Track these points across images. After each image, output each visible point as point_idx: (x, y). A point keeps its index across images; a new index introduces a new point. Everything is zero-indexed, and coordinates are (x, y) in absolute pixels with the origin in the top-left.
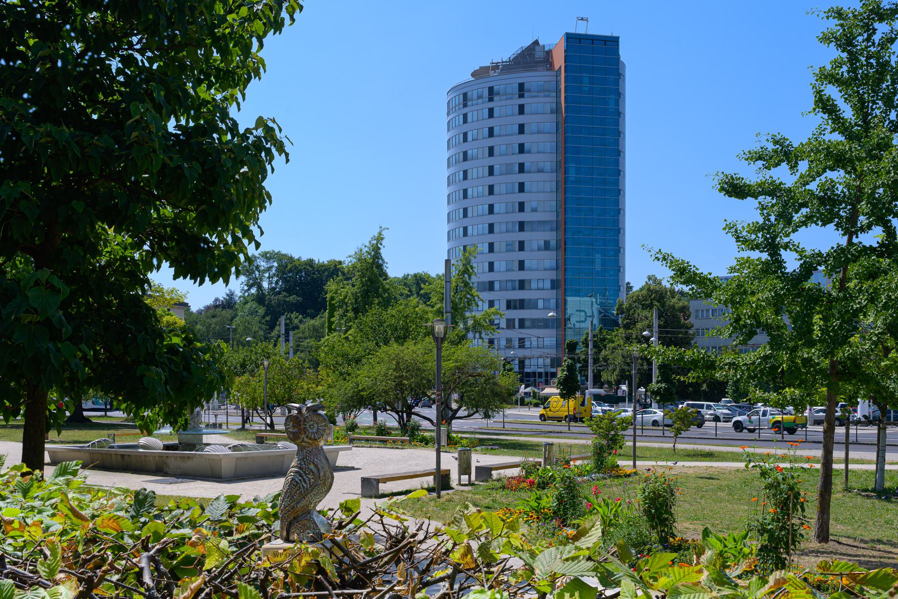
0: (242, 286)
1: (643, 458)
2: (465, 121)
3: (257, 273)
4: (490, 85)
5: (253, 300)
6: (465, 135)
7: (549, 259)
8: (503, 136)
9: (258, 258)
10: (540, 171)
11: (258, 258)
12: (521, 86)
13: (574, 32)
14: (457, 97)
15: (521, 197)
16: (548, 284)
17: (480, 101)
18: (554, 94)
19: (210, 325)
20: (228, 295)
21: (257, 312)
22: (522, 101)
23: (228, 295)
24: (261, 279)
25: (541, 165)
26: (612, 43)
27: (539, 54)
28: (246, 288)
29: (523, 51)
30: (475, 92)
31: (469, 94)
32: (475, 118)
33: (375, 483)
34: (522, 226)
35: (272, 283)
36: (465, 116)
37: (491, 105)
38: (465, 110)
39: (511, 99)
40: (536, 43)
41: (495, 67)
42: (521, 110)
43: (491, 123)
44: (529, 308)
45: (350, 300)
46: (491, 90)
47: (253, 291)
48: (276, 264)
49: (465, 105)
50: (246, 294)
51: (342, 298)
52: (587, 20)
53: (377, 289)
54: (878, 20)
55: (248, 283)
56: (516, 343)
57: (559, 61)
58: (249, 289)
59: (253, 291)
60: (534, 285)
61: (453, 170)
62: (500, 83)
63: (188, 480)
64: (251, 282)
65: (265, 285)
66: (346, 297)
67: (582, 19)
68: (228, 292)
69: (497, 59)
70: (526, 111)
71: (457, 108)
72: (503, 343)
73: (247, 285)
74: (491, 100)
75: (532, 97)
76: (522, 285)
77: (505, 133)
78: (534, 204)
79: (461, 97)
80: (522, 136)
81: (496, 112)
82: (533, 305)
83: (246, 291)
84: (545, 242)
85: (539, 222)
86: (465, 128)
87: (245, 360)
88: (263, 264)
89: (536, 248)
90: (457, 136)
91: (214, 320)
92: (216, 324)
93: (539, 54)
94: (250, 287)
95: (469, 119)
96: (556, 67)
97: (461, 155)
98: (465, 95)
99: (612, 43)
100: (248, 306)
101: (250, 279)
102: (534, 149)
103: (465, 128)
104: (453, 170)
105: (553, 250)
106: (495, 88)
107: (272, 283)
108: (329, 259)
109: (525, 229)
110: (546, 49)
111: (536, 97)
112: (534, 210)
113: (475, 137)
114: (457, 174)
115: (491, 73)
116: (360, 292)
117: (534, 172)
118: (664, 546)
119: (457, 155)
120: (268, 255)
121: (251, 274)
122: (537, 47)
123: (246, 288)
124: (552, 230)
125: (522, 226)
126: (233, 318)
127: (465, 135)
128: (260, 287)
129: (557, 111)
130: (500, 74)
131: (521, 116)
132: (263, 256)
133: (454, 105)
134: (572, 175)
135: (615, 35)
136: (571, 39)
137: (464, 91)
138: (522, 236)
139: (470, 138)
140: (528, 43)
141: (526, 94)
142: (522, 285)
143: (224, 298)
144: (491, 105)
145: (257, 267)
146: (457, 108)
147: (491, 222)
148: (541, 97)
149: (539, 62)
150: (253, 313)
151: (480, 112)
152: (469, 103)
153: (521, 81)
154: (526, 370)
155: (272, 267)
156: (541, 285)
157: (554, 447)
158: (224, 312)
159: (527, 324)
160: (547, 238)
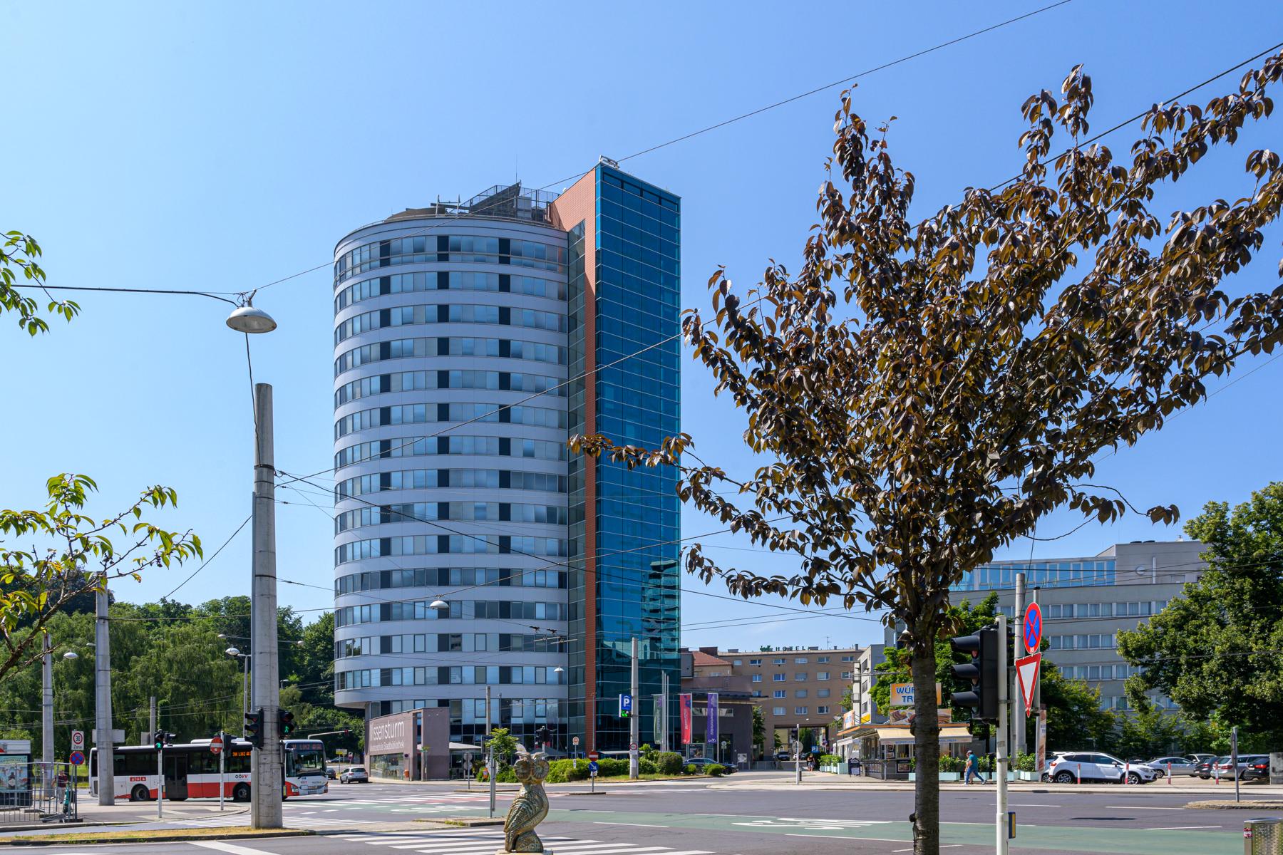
7: (550, 537)
12: (504, 245)
15: (505, 430)
16: (553, 580)
25: (542, 381)
34: (505, 479)
38: (385, 272)
42: (443, 281)
44: (519, 617)
46: (443, 242)
49: (385, 263)
54: (898, 610)
60: (528, 579)
70: (452, 284)
72: (469, 673)
75: (403, 263)
76: (505, 577)
78: (528, 445)
81: (395, 284)
82: (527, 611)
84: (549, 508)
89: (533, 517)
98: (385, 248)
102: (529, 351)
106: (451, 239)
111: (412, 262)
112: (529, 454)
125: (505, 479)
131: (443, 292)
134: (608, 397)
138: (506, 496)
141: (393, 260)
142: (505, 577)
148: (538, 268)
153: (505, 235)
154: (514, 721)
156: (540, 579)
159: (516, 643)
160: (553, 504)
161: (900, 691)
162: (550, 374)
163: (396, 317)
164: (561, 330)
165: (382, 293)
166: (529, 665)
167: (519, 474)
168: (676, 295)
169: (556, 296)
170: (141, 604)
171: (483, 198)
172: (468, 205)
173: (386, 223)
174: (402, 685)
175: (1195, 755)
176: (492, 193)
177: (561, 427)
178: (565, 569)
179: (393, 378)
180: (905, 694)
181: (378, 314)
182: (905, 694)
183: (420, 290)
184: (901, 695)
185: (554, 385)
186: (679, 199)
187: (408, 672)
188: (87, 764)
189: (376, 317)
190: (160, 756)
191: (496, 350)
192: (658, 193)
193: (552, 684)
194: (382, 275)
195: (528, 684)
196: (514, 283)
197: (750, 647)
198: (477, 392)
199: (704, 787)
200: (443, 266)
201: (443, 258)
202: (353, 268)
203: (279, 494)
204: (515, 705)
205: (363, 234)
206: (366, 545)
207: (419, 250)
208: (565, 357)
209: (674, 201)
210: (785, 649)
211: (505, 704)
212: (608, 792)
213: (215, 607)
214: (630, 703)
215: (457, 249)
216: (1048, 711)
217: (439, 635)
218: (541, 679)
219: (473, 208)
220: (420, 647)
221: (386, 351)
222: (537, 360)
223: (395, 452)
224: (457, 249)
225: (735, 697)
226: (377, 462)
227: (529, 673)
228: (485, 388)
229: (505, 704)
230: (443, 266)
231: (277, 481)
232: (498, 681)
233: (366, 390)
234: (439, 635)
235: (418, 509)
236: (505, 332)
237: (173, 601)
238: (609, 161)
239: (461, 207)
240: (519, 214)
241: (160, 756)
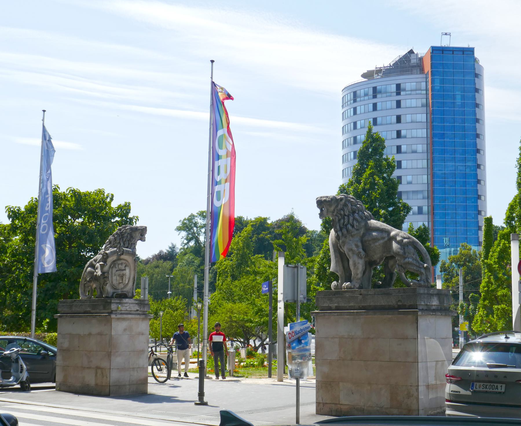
0: (183, 240)
2: (355, 113)
3: (195, 229)
4: (374, 85)
5: (191, 252)
6: (355, 124)
8: (385, 124)
11: (196, 216)
13: (440, 45)
14: (349, 95)
17: (366, 98)
18: (424, 92)
19: (153, 275)
20: (170, 248)
21: (193, 262)
22: (398, 98)
23: (170, 248)
24: (199, 234)
26: (470, 51)
27: (414, 61)
28: (186, 241)
29: (400, 59)
30: (362, 91)
31: (358, 92)
32: (363, 111)
33: (175, 364)
36: (355, 109)
37: (375, 101)
38: (355, 105)
39: (391, 96)
40: (411, 52)
41: (379, 71)
42: (398, 104)
43: (375, 114)
45: (228, 270)
46: (375, 89)
47: (192, 243)
49: (355, 101)
50: (186, 247)
51: (223, 268)
52: (450, 35)
53: (247, 262)
55: (187, 237)
57: (427, 67)
58: (188, 243)
59: (192, 243)
61: (346, 150)
62: (379, 83)
64: (190, 236)
65: (202, 238)
66: (226, 268)
67: (446, 34)
68: (171, 246)
69: (380, 65)
71: (349, 103)
73: (187, 239)
74: (375, 97)
77: (385, 123)
78: (409, 178)
79: (352, 94)
80: (399, 125)
81: (379, 106)
83: (186, 244)
85: (414, 192)
86: (355, 118)
87: (157, 310)
90: (349, 125)
91: (157, 270)
92: (158, 274)
93: (414, 61)
94: (189, 240)
95: (358, 112)
96: (426, 71)
97: (352, 139)
98: (355, 93)
99: (470, 51)
100: (186, 257)
101: (189, 234)
103: (355, 118)
104: (346, 150)
105: (426, 214)
106: (378, 87)
108: (257, 216)
110: (419, 56)
113: (363, 126)
114: (349, 154)
115: (375, 76)
116: (235, 264)
117: (409, 153)
119: (349, 139)
120: (204, 214)
121: (189, 230)
122: (412, 55)
123: (186, 241)
124: (424, 198)
126: (173, 267)
127: (355, 124)
128: (197, 241)
129: (427, 105)
130: (382, 77)
132: (200, 215)
133: (346, 101)
135: (471, 46)
136: (435, 50)
137: (354, 90)
139: (358, 126)
140: (403, 52)
143: (168, 251)
144: (375, 101)
145: (196, 224)
146: (349, 103)
149: (413, 67)
150: (190, 263)
151: (366, 106)
152: (358, 99)
158: (165, 263)
165: (354, 115)
168: (469, 395)
175: (447, 417)
183: (366, 113)
187: (363, 107)
188: (490, 366)
190: (169, 278)
202: (348, 102)
207: (366, 95)
209: (55, 151)
215: (380, 92)
216: (357, 176)
217: (397, 116)
218: (367, 111)
224: (380, 92)
234: (397, 116)
241: (169, 278)
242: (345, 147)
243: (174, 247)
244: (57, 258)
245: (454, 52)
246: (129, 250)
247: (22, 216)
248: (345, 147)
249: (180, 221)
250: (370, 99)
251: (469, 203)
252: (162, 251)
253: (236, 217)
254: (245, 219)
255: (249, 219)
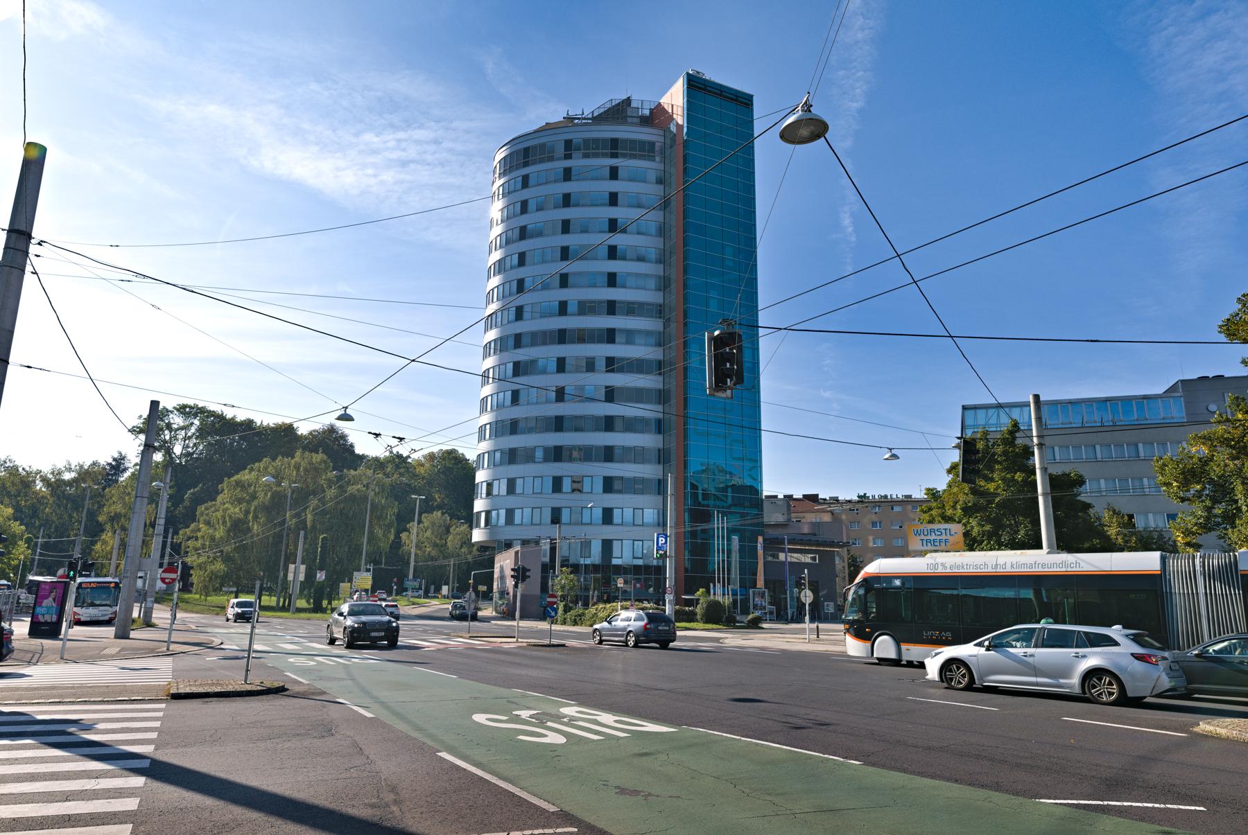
1: (1125, 455)
3: (167, 432)
9: (172, 412)
10: (641, 259)
11: (172, 412)
20: (115, 459)
32: (527, 520)
35: (188, 447)
46: (568, 144)
48: (197, 422)
56: (567, 485)
63: (1216, 717)
65: (178, 449)
68: (116, 455)
70: (619, 202)
88: (177, 420)
97: (515, 284)
107: (188, 447)
109: (617, 339)
118: (406, 463)
132: (178, 410)
143: (109, 464)
145: (169, 426)
147: (519, 277)
155: (192, 424)
157: (464, 527)
159: (617, 485)
161: (917, 533)
162: (649, 244)
163: (532, 205)
164: (661, 210)
166: (502, 496)
167: (622, 330)
169: (654, 181)
170: (374, 456)
171: (602, 110)
172: (590, 116)
173: (536, 132)
174: (540, 524)
176: (608, 106)
177: (656, 290)
178: (661, 416)
179: (527, 254)
180: (923, 537)
181: (519, 204)
182: (923, 537)
184: (919, 538)
185: (653, 255)
186: (752, 96)
187: (527, 511)
189: (518, 206)
191: (606, 227)
192: (734, 93)
193: (648, 525)
194: (524, 174)
195: (628, 525)
196: (621, 173)
197: (849, 494)
198: (590, 262)
199: (717, 640)
200: (567, 163)
201: (568, 157)
203: (33, 262)
204: (616, 545)
205: (522, 139)
206: (501, 395)
208: (662, 231)
210: (906, 496)
211: (607, 545)
212: (569, 643)
213: (431, 457)
214: (666, 542)
219: (593, 119)
220: (537, 490)
221: (523, 233)
222: (639, 233)
223: (526, 315)
225: (825, 544)
226: (513, 324)
227: (628, 513)
228: (596, 259)
229: (607, 545)
230: (567, 163)
231: (33, 249)
232: (601, 522)
233: (508, 265)
235: (541, 363)
236: (614, 212)
237: (398, 452)
238: (698, 72)
239: (584, 119)
240: (629, 120)
242: (483, 438)
243: (123, 458)
244: (630, 493)
245: (521, 510)
246: (297, 485)
247: (352, 489)
248: (483, 438)
249: (141, 417)
250: (535, 318)
251: (1200, 799)
252: (97, 463)
253: (239, 421)
254: (259, 424)
255: (265, 424)
